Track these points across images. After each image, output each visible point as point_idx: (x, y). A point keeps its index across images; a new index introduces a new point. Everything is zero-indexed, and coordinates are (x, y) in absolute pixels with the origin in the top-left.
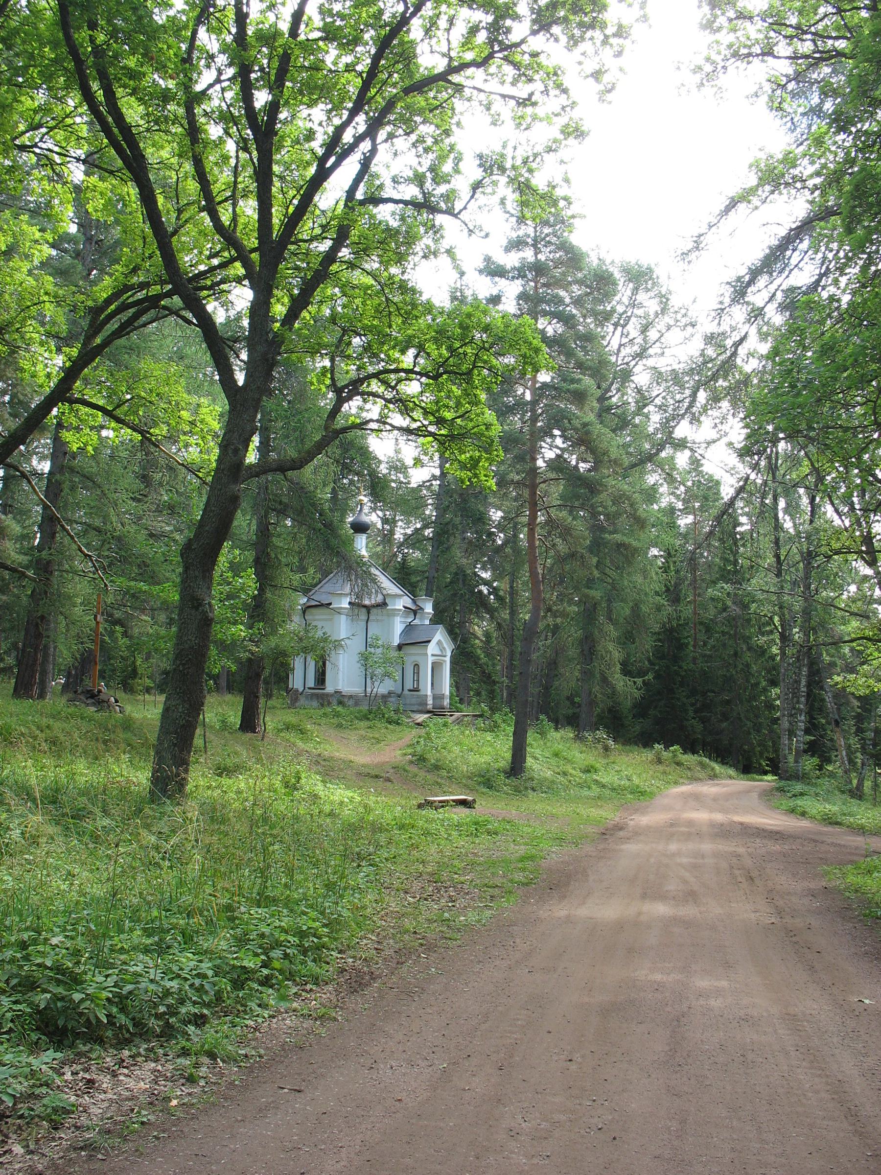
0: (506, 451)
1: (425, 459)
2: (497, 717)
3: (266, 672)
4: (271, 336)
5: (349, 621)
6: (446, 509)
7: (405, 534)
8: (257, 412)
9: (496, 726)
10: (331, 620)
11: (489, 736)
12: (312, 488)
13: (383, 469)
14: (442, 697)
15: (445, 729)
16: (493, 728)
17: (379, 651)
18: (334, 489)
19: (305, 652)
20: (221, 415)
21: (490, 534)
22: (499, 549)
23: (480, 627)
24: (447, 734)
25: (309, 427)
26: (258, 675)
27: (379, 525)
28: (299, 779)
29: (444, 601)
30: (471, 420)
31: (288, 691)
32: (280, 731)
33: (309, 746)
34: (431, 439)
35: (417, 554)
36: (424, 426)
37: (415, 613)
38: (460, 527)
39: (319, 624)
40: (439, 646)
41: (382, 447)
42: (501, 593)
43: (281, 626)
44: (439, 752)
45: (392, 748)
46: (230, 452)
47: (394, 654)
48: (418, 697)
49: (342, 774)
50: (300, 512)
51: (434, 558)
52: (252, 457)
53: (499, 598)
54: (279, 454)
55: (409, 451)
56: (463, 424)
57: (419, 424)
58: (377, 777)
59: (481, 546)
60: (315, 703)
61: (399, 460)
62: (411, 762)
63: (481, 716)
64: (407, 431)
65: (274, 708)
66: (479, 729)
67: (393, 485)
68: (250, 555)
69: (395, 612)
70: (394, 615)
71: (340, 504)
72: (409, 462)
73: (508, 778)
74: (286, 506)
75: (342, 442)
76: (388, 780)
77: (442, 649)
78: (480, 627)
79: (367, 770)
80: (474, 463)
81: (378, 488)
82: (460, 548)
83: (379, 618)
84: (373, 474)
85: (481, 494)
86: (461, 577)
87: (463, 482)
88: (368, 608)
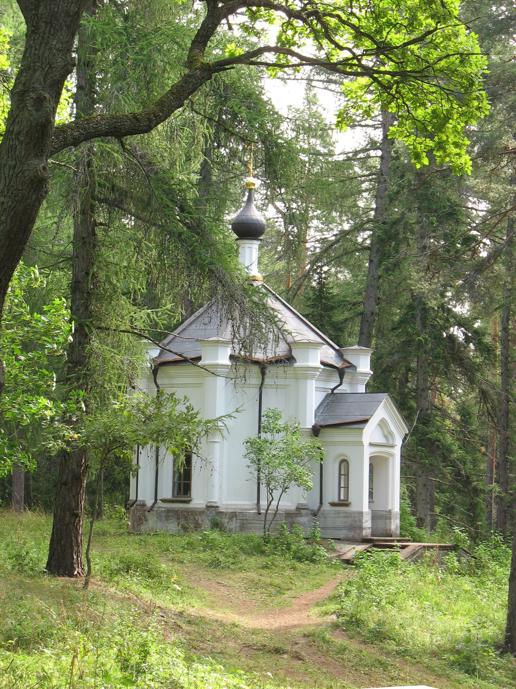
0: (494, 98)
1: (355, 114)
2: (481, 550)
3: (93, 473)
5: (230, 386)
6: (392, 199)
7: (323, 241)
8: (73, 35)
9: (480, 566)
10: (200, 385)
11: (467, 584)
12: (166, 164)
13: (286, 131)
14: (387, 516)
15: (392, 570)
16: (475, 569)
17: (278, 437)
18: (204, 164)
19: (156, 440)
20: (14, 41)
21: (468, 240)
22: (482, 267)
23: (451, 398)
24: (394, 580)
25: (158, 57)
26: (78, 479)
27: (280, 225)
28: (145, 654)
29: (391, 354)
30: (436, 47)
31: (128, 504)
32: (113, 573)
33: (163, 600)
34: (365, 80)
35: (345, 275)
36: (355, 57)
37: (341, 373)
38: (417, 227)
39: (179, 395)
40: (383, 428)
41: (283, 94)
42: (488, 340)
43: (115, 397)
44: (382, 609)
45: (304, 606)
46: (29, 103)
47: (306, 442)
48: (348, 515)
49: (219, 646)
50: (145, 204)
51: (374, 282)
52: (64, 113)
53: (485, 350)
54: (108, 106)
55: (329, 102)
56: (422, 53)
57: (346, 54)
58: (278, 651)
59: (453, 258)
60: (173, 526)
61: (313, 115)
62: (335, 626)
63: (454, 548)
64: (327, 66)
65: (104, 533)
66: (450, 571)
67: (304, 157)
68: (64, 277)
69: (307, 373)
70: (306, 377)
71: (213, 188)
72: (330, 118)
73: (501, 655)
74: (124, 194)
75: (212, 83)
76: (298, 657)
77: (388, 435)
78: (451, 398)
79: (259, 639)
80: (440, 121)
81: (276, 162)
82: (417, 263)
83: (280, 382)
84: (269, 140)
85: (449, 174)
86: (418, 313)
87: (417, 156)
88: (262, 366)
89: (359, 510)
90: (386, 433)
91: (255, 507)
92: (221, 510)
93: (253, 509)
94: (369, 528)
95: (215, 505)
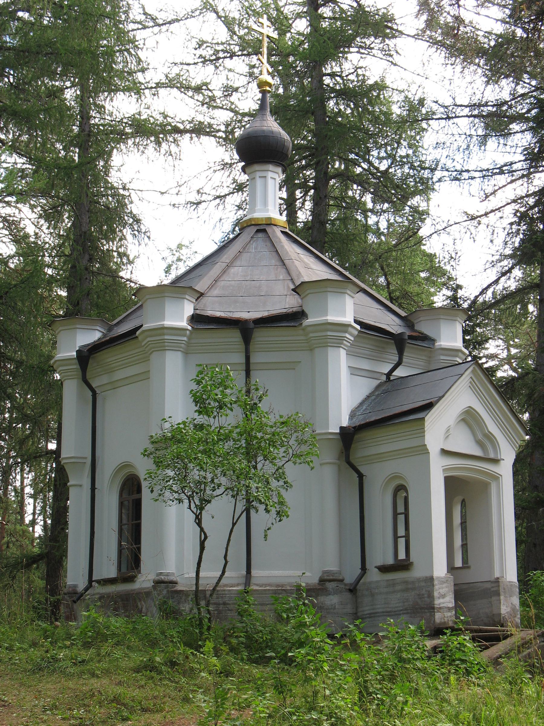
4: (537, 198)
14: (494, 589)
48: (409, 586)
89: (428, 575)
90: (480, 436)
91: (243, 580)
92: (179, 588)
93: (238, 585)
94: (449, 609)
95: (172, 578)
